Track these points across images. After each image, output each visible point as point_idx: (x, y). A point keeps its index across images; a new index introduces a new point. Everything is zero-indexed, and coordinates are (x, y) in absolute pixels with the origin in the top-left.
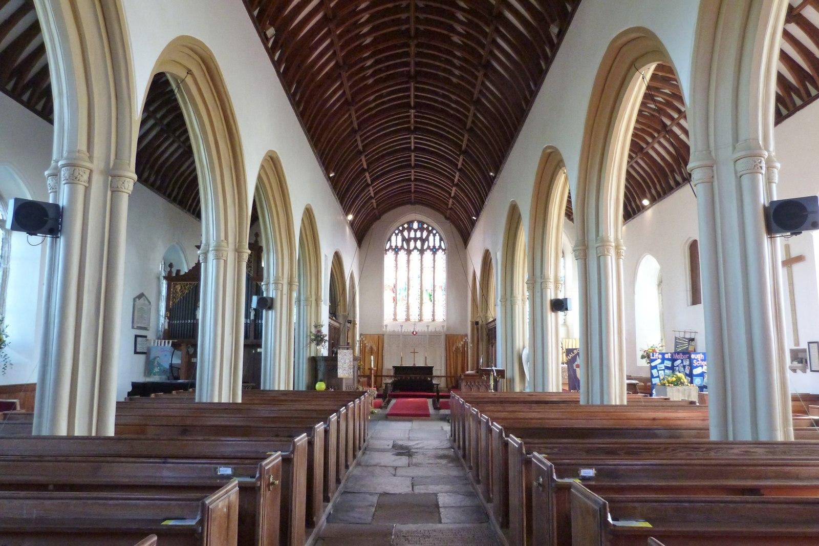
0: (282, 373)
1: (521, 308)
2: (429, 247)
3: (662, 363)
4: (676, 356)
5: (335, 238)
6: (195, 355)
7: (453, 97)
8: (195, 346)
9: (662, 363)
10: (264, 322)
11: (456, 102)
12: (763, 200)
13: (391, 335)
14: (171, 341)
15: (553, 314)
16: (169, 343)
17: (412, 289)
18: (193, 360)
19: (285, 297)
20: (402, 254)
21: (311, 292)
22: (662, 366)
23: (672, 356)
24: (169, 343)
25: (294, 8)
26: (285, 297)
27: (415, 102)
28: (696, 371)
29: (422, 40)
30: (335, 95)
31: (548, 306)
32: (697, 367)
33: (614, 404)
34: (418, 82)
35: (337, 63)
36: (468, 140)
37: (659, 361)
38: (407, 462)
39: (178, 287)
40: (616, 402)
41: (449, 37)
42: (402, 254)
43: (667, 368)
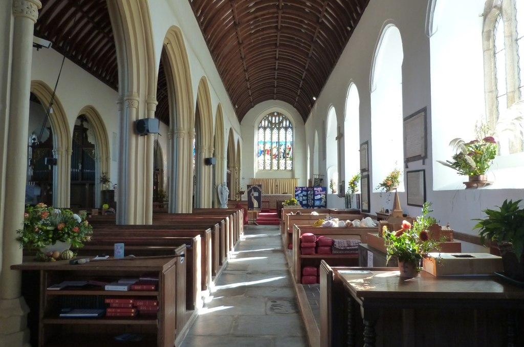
0: (206, 203)
1: (220, 162)
2: (283, 127)
3: (302, 192)
4: (309, 189)
5: (230, 119)
6: (51, 189)
7: (303, 41)
8: (51, 185)
9: (302, 192)
10: (96, 171)
11: (304, 43)
12: (134, 119)
13: (73, 178)
14: (34, 183)
15: (206, 167)
16: (33, 183)
17: (269, 148)
18: (37, 192)
19: (64, 158)
20: (268, 131)
21: (102, 153)
22: (301, 195)
23: (307, 189)
24: (33, 183)
25: (63, 23)
26: (64, 158)
27: (280, 43)
28: (316, 198)
29: (285, 10)
30: (231, 42)
31: (203, 161)
32: (318, 195)
33: (180, 213)
34: (282, 33)
35: (235, 22)
36: (310, 63)
37: (300, 191)
38: (282, 261)
39: (39, 152)
40: (182, 210)
41: (304, 9)
42: (268, 131)
43: (304, 195)
